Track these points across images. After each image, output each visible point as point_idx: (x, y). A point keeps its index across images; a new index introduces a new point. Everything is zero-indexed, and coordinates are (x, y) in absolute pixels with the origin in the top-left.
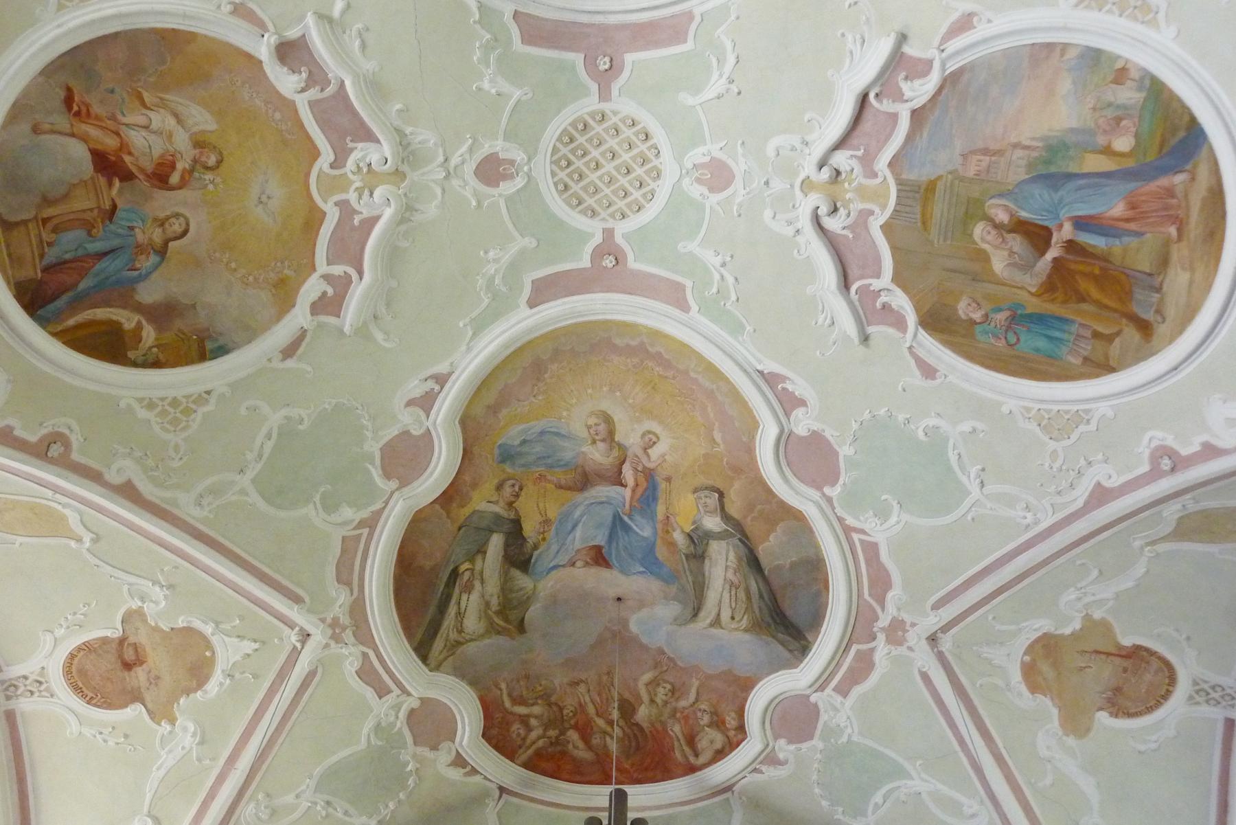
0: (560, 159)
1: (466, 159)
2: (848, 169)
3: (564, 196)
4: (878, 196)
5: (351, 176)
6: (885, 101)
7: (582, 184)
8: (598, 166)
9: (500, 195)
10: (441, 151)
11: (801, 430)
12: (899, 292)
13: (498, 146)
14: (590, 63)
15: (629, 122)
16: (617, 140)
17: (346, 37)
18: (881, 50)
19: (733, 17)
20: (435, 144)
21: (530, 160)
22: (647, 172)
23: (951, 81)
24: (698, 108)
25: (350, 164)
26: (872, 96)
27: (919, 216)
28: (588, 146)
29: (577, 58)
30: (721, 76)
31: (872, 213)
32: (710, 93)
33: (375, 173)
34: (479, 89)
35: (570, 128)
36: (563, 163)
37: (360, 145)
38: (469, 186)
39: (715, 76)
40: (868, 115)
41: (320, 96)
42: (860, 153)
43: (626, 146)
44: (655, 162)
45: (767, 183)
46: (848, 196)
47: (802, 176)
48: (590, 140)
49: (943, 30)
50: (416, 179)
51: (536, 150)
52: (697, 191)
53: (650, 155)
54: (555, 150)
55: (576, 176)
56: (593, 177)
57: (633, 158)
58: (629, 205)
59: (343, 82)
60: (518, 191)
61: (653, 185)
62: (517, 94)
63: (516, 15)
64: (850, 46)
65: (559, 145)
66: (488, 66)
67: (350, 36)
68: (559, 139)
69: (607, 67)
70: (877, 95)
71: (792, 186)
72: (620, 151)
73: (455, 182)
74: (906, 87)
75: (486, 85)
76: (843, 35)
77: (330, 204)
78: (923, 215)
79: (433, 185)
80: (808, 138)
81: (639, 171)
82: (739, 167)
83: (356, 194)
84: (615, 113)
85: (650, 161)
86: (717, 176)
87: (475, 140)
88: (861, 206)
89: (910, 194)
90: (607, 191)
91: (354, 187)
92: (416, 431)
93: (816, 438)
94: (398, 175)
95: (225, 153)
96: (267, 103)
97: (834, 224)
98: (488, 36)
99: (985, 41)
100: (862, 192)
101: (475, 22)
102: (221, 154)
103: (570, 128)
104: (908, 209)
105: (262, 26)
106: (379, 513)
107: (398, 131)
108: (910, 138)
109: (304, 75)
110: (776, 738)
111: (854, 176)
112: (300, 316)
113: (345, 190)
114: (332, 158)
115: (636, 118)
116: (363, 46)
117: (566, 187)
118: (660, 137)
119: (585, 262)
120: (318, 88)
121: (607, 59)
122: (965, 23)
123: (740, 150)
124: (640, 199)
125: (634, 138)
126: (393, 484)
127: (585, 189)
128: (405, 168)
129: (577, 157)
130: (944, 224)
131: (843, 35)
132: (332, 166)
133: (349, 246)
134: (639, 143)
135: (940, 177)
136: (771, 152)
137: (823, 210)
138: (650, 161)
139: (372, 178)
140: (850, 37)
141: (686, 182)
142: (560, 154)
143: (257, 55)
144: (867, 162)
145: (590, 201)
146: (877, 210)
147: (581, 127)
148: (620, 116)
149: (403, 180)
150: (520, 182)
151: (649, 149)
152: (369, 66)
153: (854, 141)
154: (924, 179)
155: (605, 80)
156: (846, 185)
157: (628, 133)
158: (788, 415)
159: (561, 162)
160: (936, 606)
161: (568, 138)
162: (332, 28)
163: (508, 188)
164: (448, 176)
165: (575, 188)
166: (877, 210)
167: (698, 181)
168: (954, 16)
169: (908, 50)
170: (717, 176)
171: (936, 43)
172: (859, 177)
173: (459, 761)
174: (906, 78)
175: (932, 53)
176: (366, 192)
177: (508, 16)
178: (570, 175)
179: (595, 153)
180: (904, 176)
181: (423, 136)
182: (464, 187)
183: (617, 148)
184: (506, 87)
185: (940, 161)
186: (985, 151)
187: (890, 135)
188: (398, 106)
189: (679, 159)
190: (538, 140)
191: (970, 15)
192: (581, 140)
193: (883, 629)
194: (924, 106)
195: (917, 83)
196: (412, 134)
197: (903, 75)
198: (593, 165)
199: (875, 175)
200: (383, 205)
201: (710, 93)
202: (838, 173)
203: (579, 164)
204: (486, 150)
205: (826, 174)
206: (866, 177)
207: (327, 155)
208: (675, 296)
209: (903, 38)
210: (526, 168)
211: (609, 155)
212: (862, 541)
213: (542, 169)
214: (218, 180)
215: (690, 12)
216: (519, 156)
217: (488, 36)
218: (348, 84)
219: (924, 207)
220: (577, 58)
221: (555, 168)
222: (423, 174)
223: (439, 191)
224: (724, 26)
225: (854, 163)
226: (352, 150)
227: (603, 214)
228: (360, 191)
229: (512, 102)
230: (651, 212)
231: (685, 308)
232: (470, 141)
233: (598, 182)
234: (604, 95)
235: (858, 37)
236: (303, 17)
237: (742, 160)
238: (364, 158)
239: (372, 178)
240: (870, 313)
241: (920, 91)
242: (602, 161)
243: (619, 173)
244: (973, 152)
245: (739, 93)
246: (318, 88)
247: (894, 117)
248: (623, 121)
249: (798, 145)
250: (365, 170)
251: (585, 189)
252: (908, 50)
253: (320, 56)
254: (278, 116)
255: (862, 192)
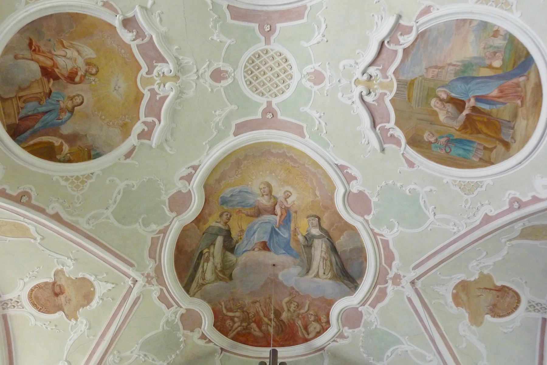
0: (248, 70)
1: (206, 70)
2: (375, 75)
3: (250, 87)
4: (389, 87)
5: (155, 78)
6: (392, 45)
7: (258, 81)
8: (265, 73)
9: (221, 86)
10: (195, 67)
11: (355, 190)
12: (398, 129)
13: (220, 65)
14: (261, 28)
15: (279, 54)
16: (273, 62)
17: (153, 16)
18: (390, 22)
19: (324, 8)
20: (193, 64)
21: (234, 71)
22: (287, 76)
23: (421, 36)
24: (309, 48)
25: (155, 72)
26: (386, 42)
27: (407, 96)
28: (260, 65)
29: (255, 26)
30: (319, 33)
31: (386, 94)
32: (314, 41)
33: (166, 76)
34: (212, 39)
35: (252, 57)
36: (249, 72)
37: (159, 64)
38: (207, 82)
39: (317, 34)
40: (384, 51)
41: (142, 42)
42: (381, 68)
43: (277, 65)
44: (290, 72)
45: (339, 81)
46: (375, 87)
47: (355, 78)
48: (261, 62)
49: (417, 13)
50: (184, 79)
51: (237, 66)
52: (308, 85)
53: (288, 68)
54: (246, 66)
55: (255, 78)
56: (263, 78)
57: (280, 70)
58: (278, 91)
59: (152, 36)
60: (229, 84)
61: (289, 82)
62: (229, 42)
63: (229, 7)
64: (376, 20)
65: (247, 64)
66: (216, 29)
67: (155, 16)
68: (248, 62)
69: (268, 29)
70: (388, 42)
71: (351, 82)
72: (275, 67)
73: (201, 81)
74: (401, 39)
75: (215, 38)
76: (373, 16)
77: (146, 90)
78: (409, 95)
79: (192, 82)
80: (358, 61)
81: (283, 76)
82: (327, 74)
83: (158, 86)
84: (272, 50)
85: (288, 71)
86: (318, 78)
87: (210, 62)
88: (381, 91)
89: (403, 86)
90: (269, 84)
91: (156, 83)
92: (184, 191)
93: (361, 194)
94: (176, 77)
95: (99, 68)
96: (118, 45)
97: (369, 99)
98: (216, 16)
99: (436, 18)
100: (381, 85)
101: (210, 10)
102: (98, 68)
103: (252, 57)
104: (402, 93)
105: (116, 11)
106: (168, 227)
107: (176, 58)
108: (403, 61)
109: (135, 33)
110: (343, 327)
111: (378, 78)
112: (133, 140)
113: (153, 84)
114: (147, 70)
115: (282, 52)
116: (161, 20)
117: (251, 83)
118: (292, 61)
119: (259, 116)
120: (141, 39)
121: (269, 26)
122: (427, 10)
123: (327, 66)
124: (283, 88)
125: (281, 61)
126: (174, 214)
127: (259, 84)
128: (179, 74)
129: (255, 69)
130: (418, 99)
131: (373, 16)
132: (147, 74)
133: (155, 109)
134: (283, 63)
135: (416, 78)
136: (341, 67)
137: (364, 93)
138: (288, 71)
139: (164, 79)
140: (376, 16)
141: (304, 80)
142: (248, 68)
143: (114, 24)
144: (384, 72)
145: (261, 89)
146: (388, 93)
147: (257, 56)
148: (274, 51)
149: (178, 80)
150: (230, 81)
151: (287, 66)
152: (163, 29)
153: (378, 62)
154: (409, 79)
155: (268, 35)
156: (375, 82)
157: (278, 59)
158: (349, 184)
159: (248, 72)
160: (414, 268)
161: (251, 61)
162: (147, 12)
163: (225, 83)
164: (198, 78)
165: (255, 83)
166: (388, 93)
167: (309, 80)
168: (422, 7)
169: (402, 22)
170: (318, 78)
171: (414, 19)
172: (380, 78)
173: (203, 337)
174: (401, 35)
175: (412, 23)
176: (162, 85)
177: (225, 7)
178: (252, 78)
179: (263, 68)
180: (400, 78)
181: (187, 60)
182: (205, 83)
183: (273, 65)
184: (224, 38)
185: (416, 71)
186: (436, 67)
187: (394, 60)
188: (176, 47)
189: (301, 71)
190: (238, 62)
191: (429, 7)
192: (257, 62)
193: (391, 278)
194: (409, 47)
195: (406, 37)
196: (182, 59)
197: (399, 33)
198: (262, 73)
199: (387, 78)
200: (169, 91)
201: (314, 41)
202: (371, 76)
203: (256, 72)
204: (215, 66)
205: (365, 77)
206: (383, 78)
207: (145, 68)
208: (299, 131)
209: (399, 17)
210: (233, 75)
211: (270, 69)
212: (381, 239)
213: (240, 75)
214: (97, 80)
215: (306, 5)
216: (230, 69)
217: (216, 16)
218: (154, 37)
219: (409, 91)
220: (255, 26)
221: (246, 74)
222: (187, 77)
223: (194, 85)
224: (320, 12)
225: (378, 72)
226: (156, 66)
227: (267, 95)
228: (159, 85)
229: (227, 45)
230: (288, 94)
231: (303, 136)
232: (208, 62)
233: (264, 80)
234: (267, 42)
235: (380, 16)
236: (134, 8)
237: (328, 71)
238: (161, 70)
239: (164, 79)
240: (385, 138)
241: (407, 40)
242: (266, 71)
243: (274, 77)
244: (431, 67)
245: (327, 41)
246: (141, 39)
247: (396, 52)
248: (276, 53)
249: (353, 64)
250: (162, 75)
251: (259, 84)
252: (402, 22)
253: (142, 25)
254: (123, 51)
255: (381, 85)
